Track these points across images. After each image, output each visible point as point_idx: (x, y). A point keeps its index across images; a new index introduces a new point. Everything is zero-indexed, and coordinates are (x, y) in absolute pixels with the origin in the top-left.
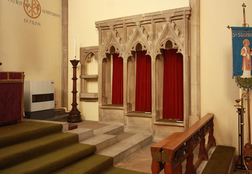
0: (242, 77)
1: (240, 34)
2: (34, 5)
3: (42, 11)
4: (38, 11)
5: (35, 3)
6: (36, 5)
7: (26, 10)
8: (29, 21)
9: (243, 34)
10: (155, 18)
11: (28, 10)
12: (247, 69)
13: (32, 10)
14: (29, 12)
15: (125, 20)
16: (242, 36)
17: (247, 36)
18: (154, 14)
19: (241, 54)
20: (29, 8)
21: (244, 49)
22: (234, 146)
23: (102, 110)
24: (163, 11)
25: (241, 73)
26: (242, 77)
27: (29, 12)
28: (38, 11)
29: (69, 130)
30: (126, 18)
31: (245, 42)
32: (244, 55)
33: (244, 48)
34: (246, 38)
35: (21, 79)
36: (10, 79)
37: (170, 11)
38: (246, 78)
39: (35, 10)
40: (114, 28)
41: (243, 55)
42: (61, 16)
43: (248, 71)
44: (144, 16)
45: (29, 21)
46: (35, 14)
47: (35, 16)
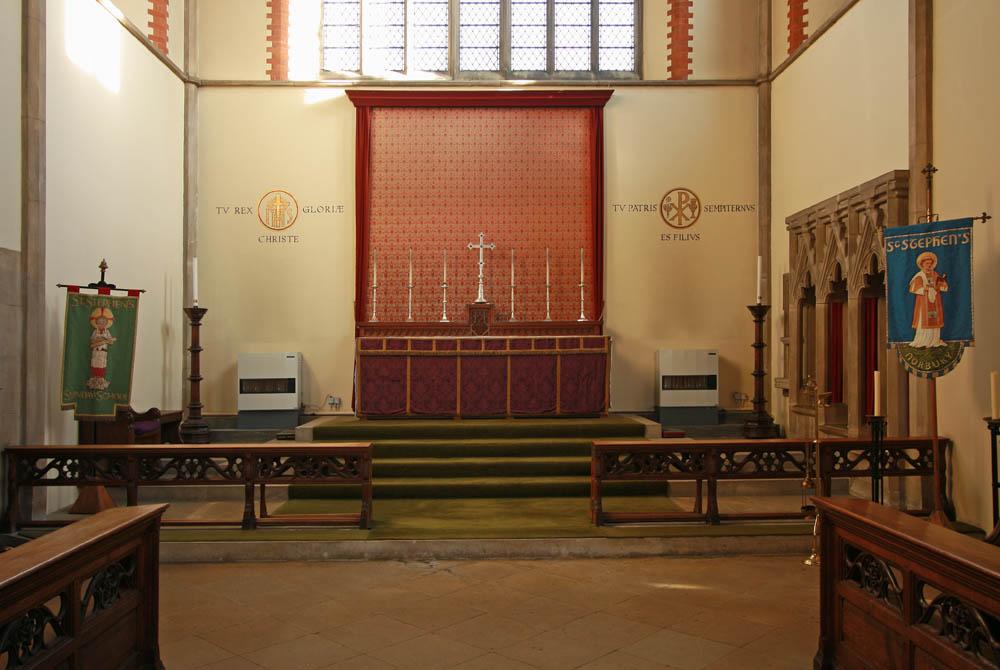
0: (912, 344)
1: (908, 243)
2: (684, 202)
3: (703, 209)
4: (693, 212)
5: (687, 197)
6: (689, 202)
7: (665, 216)
8: (672, 237)
9: (917, 242)
10: (853, 202)
11: (671, 216)
12: (931, 323)
13: (680, 214)
14: (673, 219)
15: (820, 210)
16: (912, 248)
17: (931, 245)
18: (851, 194)
19: (912, 290)
20: (674, 212)
21: (920, 278)
22: (986, 530)
23: (797, 416)
24: (862, 185)
25: (912, 335)
26: (912, 344)
27: (673, 219)
28: (693, 212)
29: (663, 437)
30: (820, 207)
31: (923, 261)
32: (920, 291)
33: (921, 274)
34: (925, 250)
35: (584, 347)
36: (584, 347)
37: (867, 186)
38: (924, 348)
39: (687, 212)
40: (811, 229)
41: (917, 293)
42: (757, 208)
43: (929, 331)
44: (838, 199)
45: (672, 237)
46: (687, 219)
47: (685, 223)
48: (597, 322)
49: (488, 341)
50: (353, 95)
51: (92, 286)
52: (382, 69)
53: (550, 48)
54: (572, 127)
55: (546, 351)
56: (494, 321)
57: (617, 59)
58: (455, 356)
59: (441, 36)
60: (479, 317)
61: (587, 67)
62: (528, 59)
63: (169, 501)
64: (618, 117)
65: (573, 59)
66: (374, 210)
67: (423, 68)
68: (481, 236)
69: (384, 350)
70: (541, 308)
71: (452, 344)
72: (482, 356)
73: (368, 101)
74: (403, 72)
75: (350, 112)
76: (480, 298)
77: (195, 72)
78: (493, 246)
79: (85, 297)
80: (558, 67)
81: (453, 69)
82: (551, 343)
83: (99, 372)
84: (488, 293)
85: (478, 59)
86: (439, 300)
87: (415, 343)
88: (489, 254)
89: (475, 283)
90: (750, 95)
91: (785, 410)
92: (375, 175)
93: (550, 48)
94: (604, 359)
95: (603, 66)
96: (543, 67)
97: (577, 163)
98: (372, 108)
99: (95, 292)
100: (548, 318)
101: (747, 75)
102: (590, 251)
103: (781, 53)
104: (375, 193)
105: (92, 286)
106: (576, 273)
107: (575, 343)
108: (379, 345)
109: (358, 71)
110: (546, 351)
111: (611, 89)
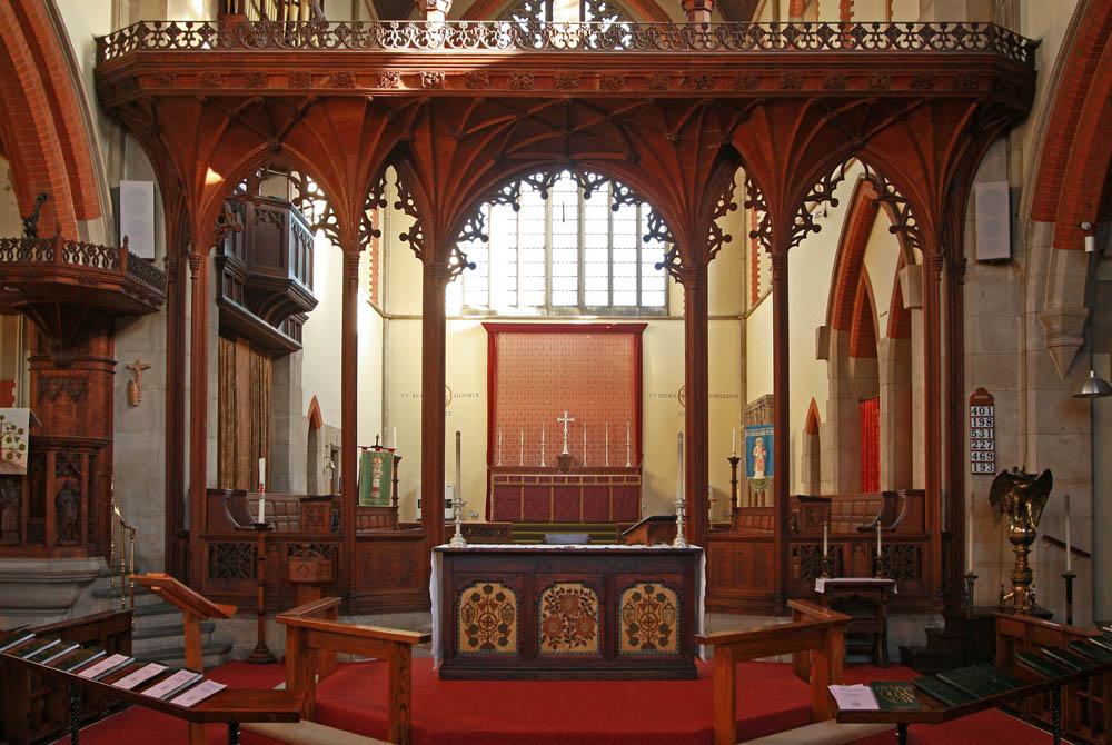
48: (638, 468)
49: (569, 478)
50: (485, 325)
51: (372, 447)
52: (506, 310)
53: (610, 291)
54: (625, 344)
55: (604, 484)
56: (573, 466)
57: (653, 299)
58: (520, 487)
59: (541, 283)
60: (564, 463)
61: (634, 303)
62: (595, 298)
63: (58, 684)
64: (648, 338)
65: (624, 298)
66: (499, 396)
67: (527, 308)
68: (566, 413)
69: (508, 482)
70: (603, 458)
71: (548, 479)
72: (596, 487)
73: (494, 330)
74: (516, 306)
75: (484, 335)
76: (565, 451)
77: (390, 311)
78: (572, 420)
79: (370, 453)
80: (615, 304)
81: (547, 306)
82: (607, 479)
83: (375, 489)
84: (571, 447)
85: (565, 297)
86: (540, 452)
87: (527, 479)
88: (571, 425)
89: (562, 442)
90: (735, 324)
91: (56, 275)
92: (500, 374)
93: (610, 291)
94: (637, 489)
95: (644, 303)
96: (606, 303)
97: (627, 367)
98: (497, 333)
99: (374, 450)
100: (607, 465)
101: (732, 313)
102: (634, 424)
103: (749, 307)
104: (499, 385)
105: (372, 447)
106: (625, 436)
107: (621, 479)
108: (505, 479)
109: (488, 306)
110: (604, 484)
111: (644, 322)
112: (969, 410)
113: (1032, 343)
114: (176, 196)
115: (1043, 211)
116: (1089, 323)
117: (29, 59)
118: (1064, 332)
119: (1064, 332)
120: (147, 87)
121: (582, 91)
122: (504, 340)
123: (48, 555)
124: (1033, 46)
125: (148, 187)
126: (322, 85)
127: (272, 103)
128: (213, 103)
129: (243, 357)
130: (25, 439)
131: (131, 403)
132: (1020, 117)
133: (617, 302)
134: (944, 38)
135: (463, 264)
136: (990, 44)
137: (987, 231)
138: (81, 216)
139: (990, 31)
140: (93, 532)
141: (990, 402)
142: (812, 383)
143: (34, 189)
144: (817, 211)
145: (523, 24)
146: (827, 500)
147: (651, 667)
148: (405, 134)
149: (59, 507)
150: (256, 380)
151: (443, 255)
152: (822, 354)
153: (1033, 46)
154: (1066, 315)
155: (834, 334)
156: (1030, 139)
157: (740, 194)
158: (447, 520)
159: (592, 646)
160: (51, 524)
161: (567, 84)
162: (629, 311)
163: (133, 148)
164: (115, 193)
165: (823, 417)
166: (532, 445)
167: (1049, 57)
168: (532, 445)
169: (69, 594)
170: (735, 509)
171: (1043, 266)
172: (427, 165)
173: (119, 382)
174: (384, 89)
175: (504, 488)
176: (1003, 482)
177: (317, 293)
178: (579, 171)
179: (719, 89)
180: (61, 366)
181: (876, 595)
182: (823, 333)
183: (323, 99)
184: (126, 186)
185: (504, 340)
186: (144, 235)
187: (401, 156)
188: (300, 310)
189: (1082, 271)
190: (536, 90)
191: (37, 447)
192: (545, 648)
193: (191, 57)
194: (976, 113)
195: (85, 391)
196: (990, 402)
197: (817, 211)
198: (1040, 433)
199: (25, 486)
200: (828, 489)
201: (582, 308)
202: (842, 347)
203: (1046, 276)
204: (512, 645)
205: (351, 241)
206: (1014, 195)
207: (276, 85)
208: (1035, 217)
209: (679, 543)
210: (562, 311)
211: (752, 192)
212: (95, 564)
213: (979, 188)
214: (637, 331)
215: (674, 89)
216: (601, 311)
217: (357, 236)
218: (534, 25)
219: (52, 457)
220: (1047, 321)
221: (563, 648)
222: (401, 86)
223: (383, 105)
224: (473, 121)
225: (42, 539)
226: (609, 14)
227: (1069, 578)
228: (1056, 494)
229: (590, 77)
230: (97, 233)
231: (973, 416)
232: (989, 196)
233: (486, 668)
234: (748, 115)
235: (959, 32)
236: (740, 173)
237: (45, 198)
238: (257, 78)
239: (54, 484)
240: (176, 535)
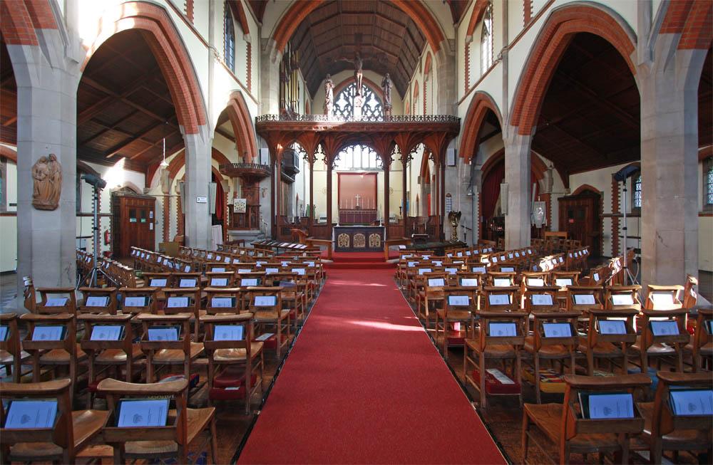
60: (357, 208)
73: (339, 174)
75: (337, 175)
97: (374, 183)
112: (446, 198)
113: (459, 183)
114: (273, 152)
115: (462, 155)
116: (472, 179)
117: (182, 75)
118: (466, 181)
119: (466, 181)
120: (268, 129)
121: (362, 130)
122: (342, 176)
123: (249, 230)
124: (460, 119)
125: (267, 150)
126: (305, 129)
127: (295, 132)
128: (283, 132)
129: (283, 185)
130: (245, 205)
131: (263, 197)
132: (458, 134)
133: (371, 167)
134: (439, 119)
135: (335, 165)
136: (449, 120)
137: (450, 159)
138: (253, 156)
139: (449, 117)
140: (256, 225)
141: (451, 196)
142: (415, 189)
143: (244, 151)
144: (413, 155)
145: (346, 93)
146: (420, 217)
147: (375, 250)
148: (323, 138)
149: (252, 220)
150: (285, 189)
151: (331, 164)
152: (419, 183)
153: (460, 119)
154: (466, 178)
155: (422, 179)
156: (459, 139)
157: (396, 151)
158: (391, 218)
159: (364, 246)
160: (250, 223)
161: (359, 129)
162: (374, 169)
163: (263, 140)
164: (260, 151)
165: (419, 198)
166: (349, 204)
167: (462, 121)
168: (349, 204)
169: (253, 238)
170: (430, 216)
171: (462, 167)
172: (328, 144)
173: (261, 192)
174: (319, 130)
175: (342, 215)
176: (451, 214)
177: (299, 169)
178: (361, 145)
179: (391, 130)
180: (249, 189)
181: (423, 238)
182: (419, 177)
183: (306, 132)
184: (262, 149)
185: (342, 176)
186: (265, 157)
187: (323, 143)
188: (296, 173)
189: (470, 168)
190: (352, 130)
191: (248, 206)
192: (355, 246)
193: (275, 123)
194: (447, 134)
195: (254, 194)
196: (451, 196)
197: (413, 155)
198: (461, 203)
199: (244, 216)
200: (420, 215)
201: (362, 168)
202: (423, 181)
203: (462, 169)
204: (348, 246)
205: (312, 161)
206: (455, 151)
207: (296, 129)
208: (460, 156)
209: (380, 226)
210: (357, 169)
211: (399, 150)
212: (259, 232)
213: (448, 150)
214: (376, 174)
215: (381, 130)
216: (367, 169)
217: (313, 160)
218: (349, 94)
219: (250, 209)
220: (462, 179)
221: (358, 246)
222: (323, 129)
223: (319, 133)
224: (339, 135)
225: (248, 226)
226: (369, 91)
227: (465, 234)
228: (462, 217)
229: (363, 128)
230: (256, 161)
231: (447, 200)
232: (450, 152)
233: (344, 250)
234: (397, 135)
235: (443, 117)
236: (396, 146)
237: (246, 153)
238: (293, 127)
239: (251, 214)
240: (274, 226)
